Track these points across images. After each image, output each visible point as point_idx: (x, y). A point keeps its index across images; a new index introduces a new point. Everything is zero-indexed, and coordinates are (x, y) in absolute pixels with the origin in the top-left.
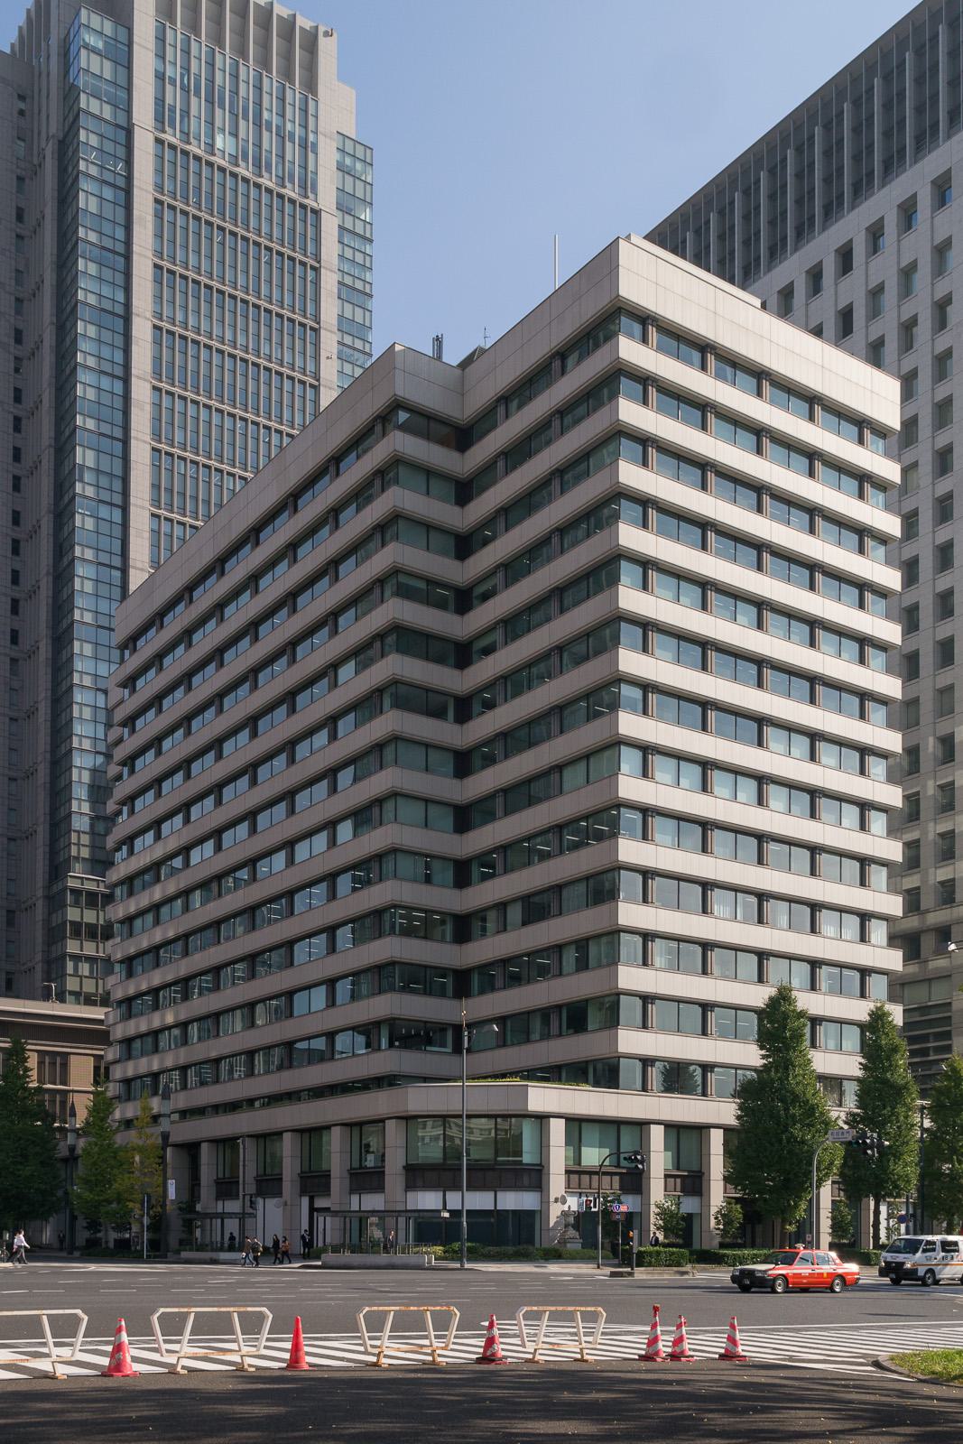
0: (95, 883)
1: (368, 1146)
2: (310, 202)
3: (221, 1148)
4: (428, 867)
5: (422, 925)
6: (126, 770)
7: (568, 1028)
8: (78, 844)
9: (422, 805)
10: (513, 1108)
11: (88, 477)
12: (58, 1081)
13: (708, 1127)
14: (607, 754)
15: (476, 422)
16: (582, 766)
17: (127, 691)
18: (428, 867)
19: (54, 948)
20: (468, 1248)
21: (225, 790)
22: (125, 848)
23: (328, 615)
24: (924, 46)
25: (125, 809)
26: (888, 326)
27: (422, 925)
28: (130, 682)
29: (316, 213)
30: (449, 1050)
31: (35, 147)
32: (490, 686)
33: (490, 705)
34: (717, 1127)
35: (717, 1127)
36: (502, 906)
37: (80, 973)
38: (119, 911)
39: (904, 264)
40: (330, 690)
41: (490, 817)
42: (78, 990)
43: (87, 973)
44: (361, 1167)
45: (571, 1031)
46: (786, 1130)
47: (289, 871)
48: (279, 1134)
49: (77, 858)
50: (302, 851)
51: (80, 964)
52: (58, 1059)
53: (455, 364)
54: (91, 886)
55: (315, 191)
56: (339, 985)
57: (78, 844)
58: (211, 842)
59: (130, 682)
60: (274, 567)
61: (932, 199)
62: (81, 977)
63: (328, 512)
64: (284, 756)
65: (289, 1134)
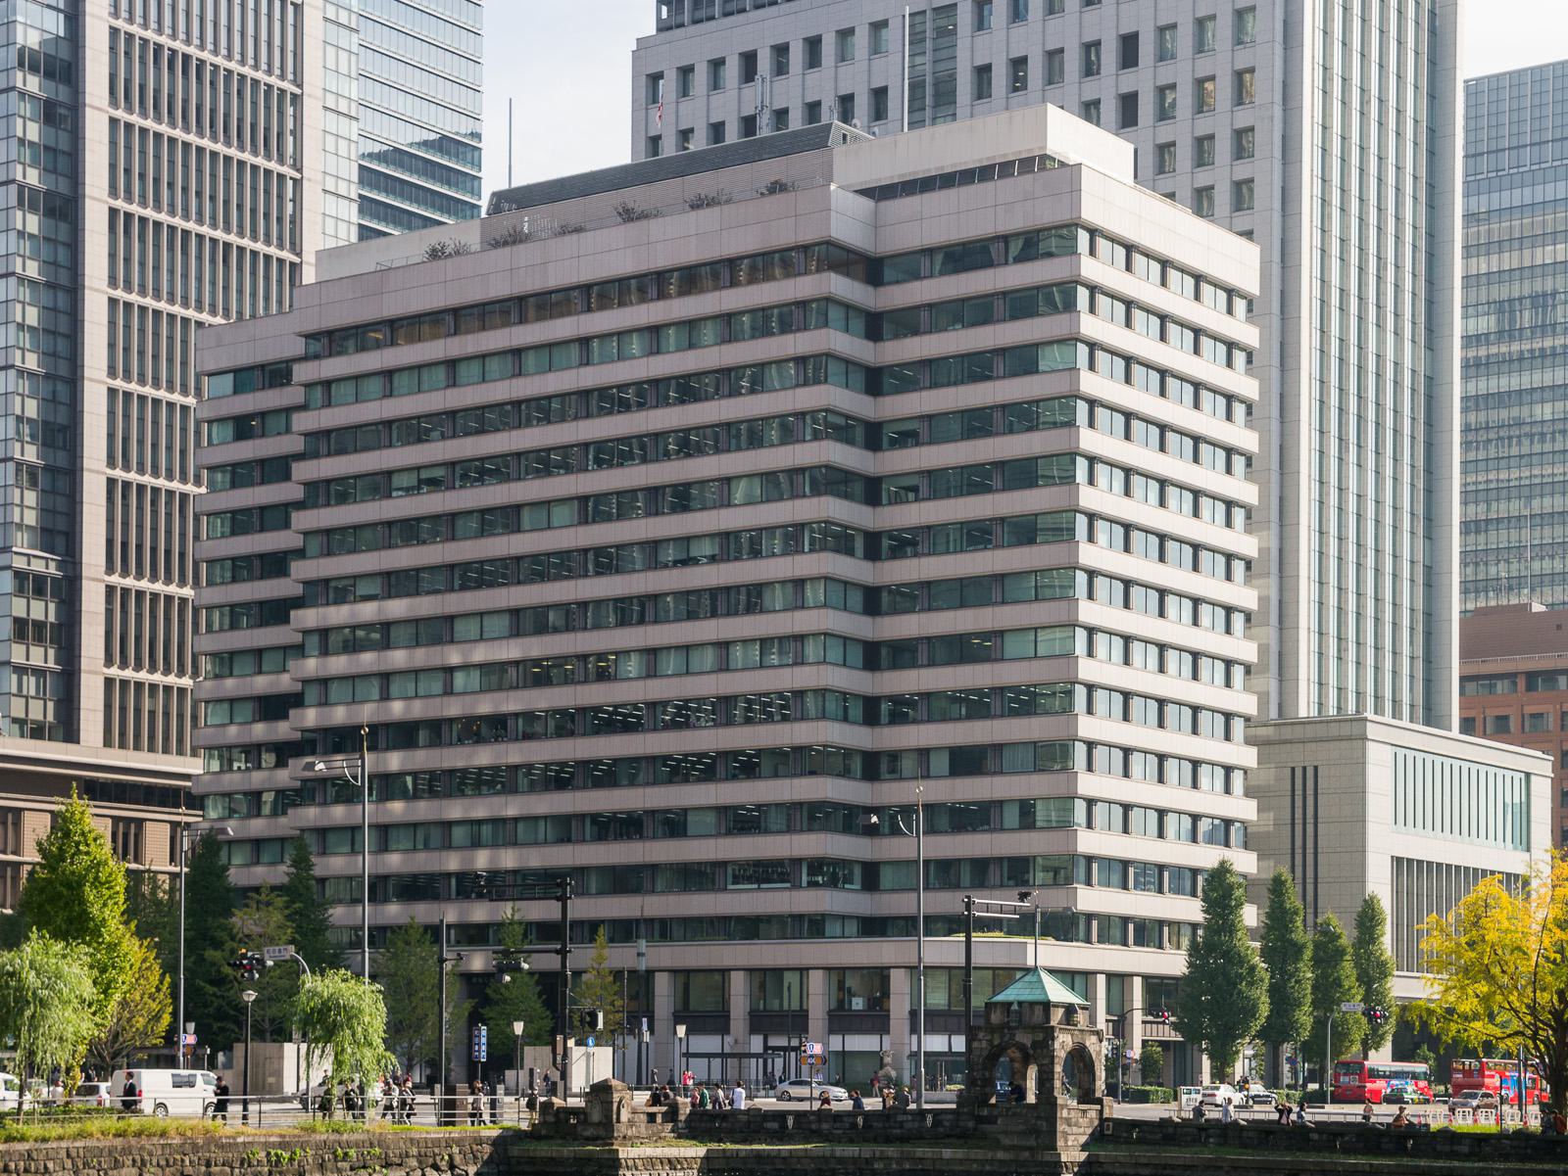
0: (43, 562)
1: (849, 989)
7: (1009, 879)
8: (21, 506)
10: (1014, 962)
12: (9, 849)
13: (1095, 973)
20: (1398, 1056)
26: (1182, 131)
30: (858, 887)
31: (679, 237)
34: (1138, 975)
35: (1138, 975)
36: (924, 753)
37: (25, 693)
42: (23, 716)
43: (33, 692)
45: (1011, 882)
46: (1235, 985)
49: (20, 526)
51: (25, 678)
52: (10, 816)
53: (654, 32)
54: (38, 566)
57: (21, 506)
62: (27, 697)
65: (742, 973)
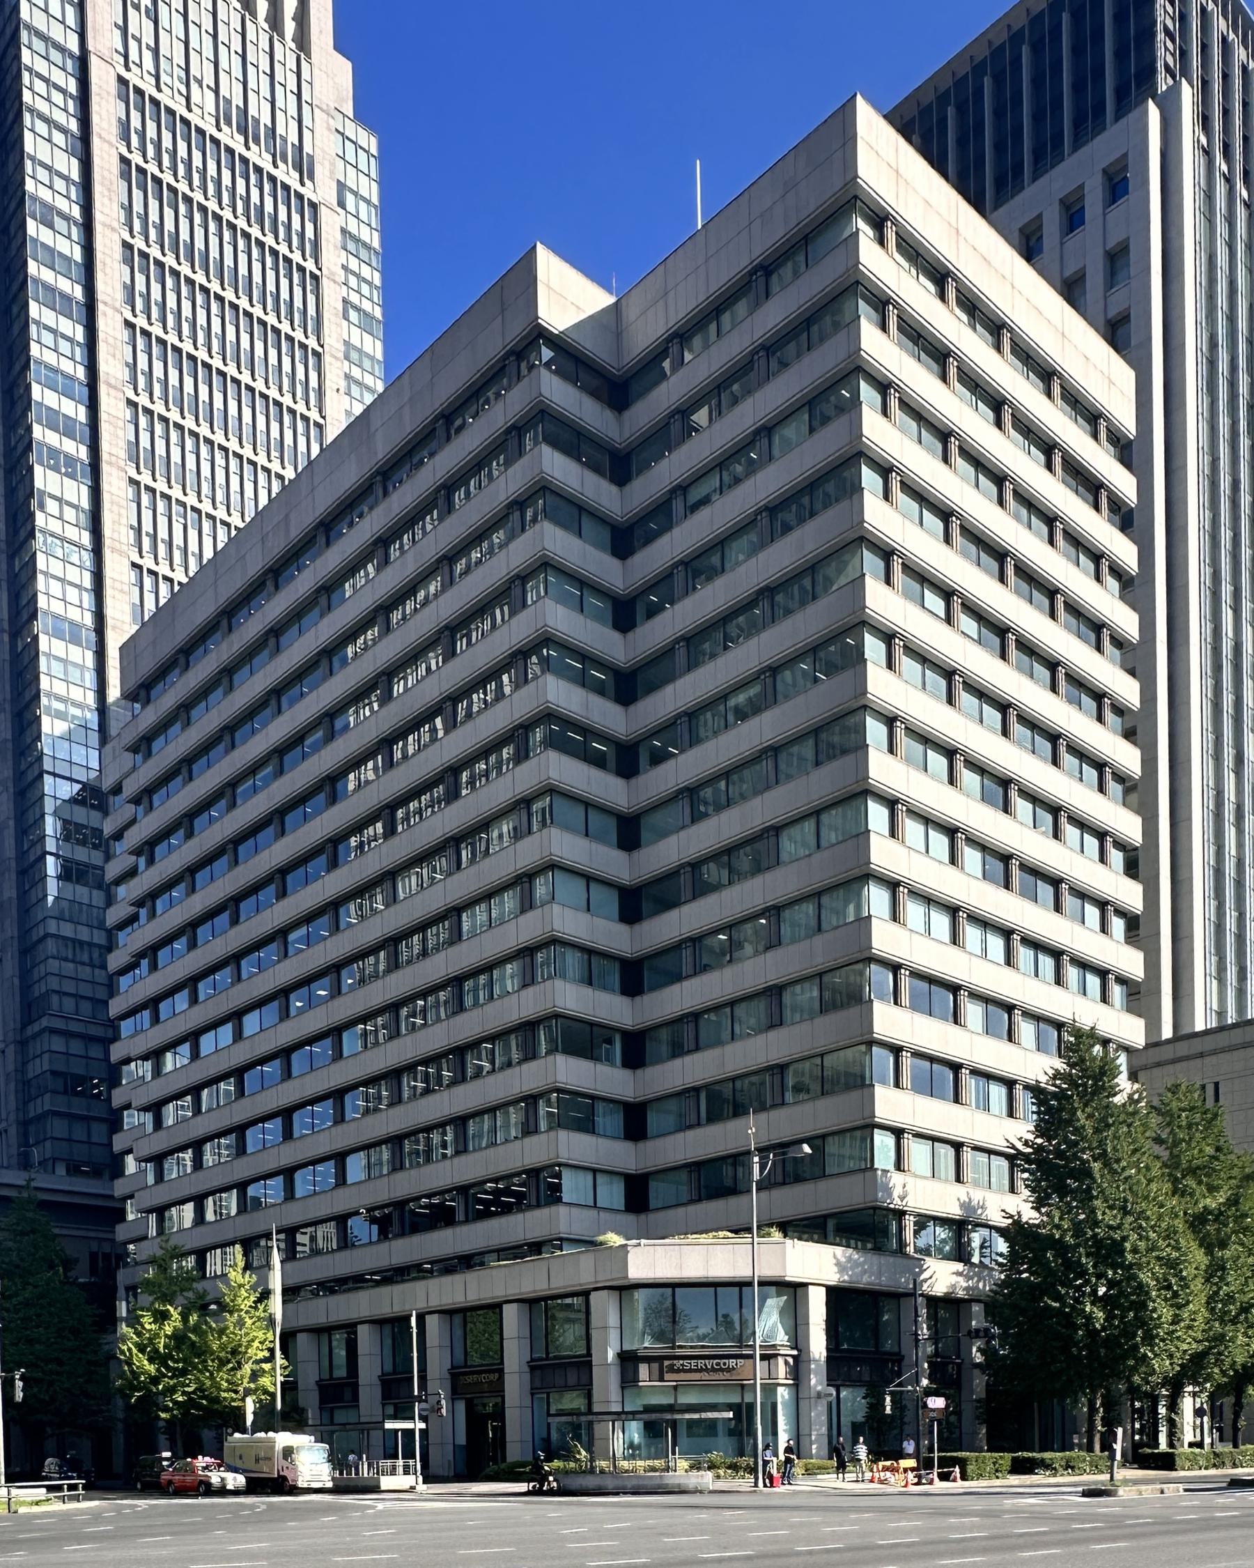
2: (307, 192)
3: (325, 1338)
4: (594, 964)
5: (583, 1038)
6: (142, 861)
9: (581, 883)
11: (52, 506)
14: (854, 803)
15: (632, 377)
16: (809, 826)
17: (139, 757)
18: (594, 964)
19: (31, 1105)
21: (160, 954)
22: (145, 963)
23: (379, 675)
24: (931, 130)
25: (143, 912)
27: (583, 1038)
28: (143, 745)
29: (314, 206)
32: (660, 730)
33: (658, 758)
38: (661, 780)
39: (1111, 244)
40: (188, 895)
41: (668, 903)
44: (331, 1378)
47: (236, 1045)
48: (496, 1308)
50: (207, 1043)
55: (311, 177)
56: (350, 1160)
58: (186, 992)
59: (143, 745)
60: (166, 730)
61: (1104, 191)
63: (438, 490)
64: (184, 940)
65: (515, 1305)
